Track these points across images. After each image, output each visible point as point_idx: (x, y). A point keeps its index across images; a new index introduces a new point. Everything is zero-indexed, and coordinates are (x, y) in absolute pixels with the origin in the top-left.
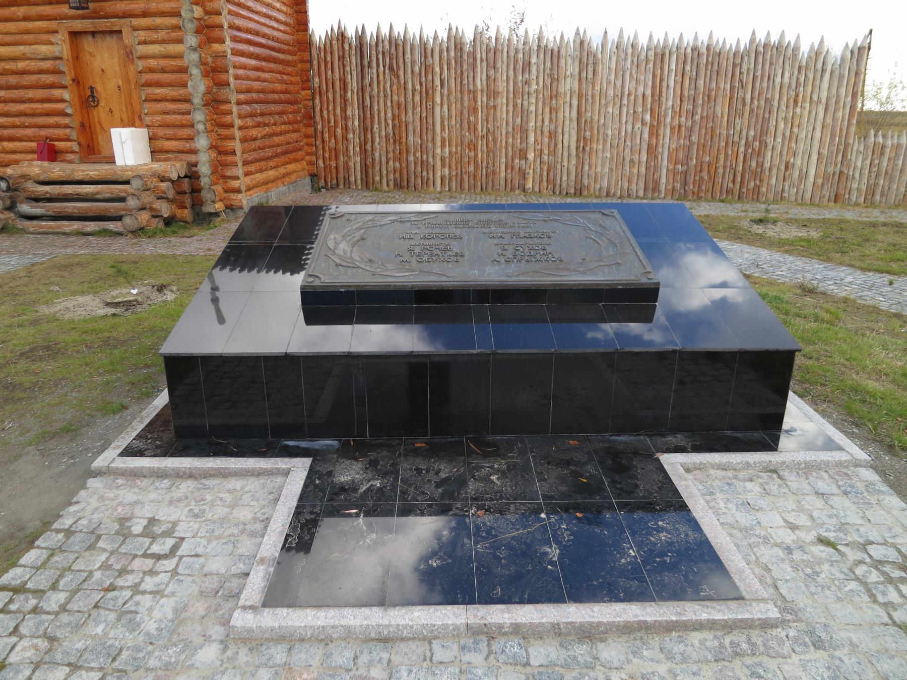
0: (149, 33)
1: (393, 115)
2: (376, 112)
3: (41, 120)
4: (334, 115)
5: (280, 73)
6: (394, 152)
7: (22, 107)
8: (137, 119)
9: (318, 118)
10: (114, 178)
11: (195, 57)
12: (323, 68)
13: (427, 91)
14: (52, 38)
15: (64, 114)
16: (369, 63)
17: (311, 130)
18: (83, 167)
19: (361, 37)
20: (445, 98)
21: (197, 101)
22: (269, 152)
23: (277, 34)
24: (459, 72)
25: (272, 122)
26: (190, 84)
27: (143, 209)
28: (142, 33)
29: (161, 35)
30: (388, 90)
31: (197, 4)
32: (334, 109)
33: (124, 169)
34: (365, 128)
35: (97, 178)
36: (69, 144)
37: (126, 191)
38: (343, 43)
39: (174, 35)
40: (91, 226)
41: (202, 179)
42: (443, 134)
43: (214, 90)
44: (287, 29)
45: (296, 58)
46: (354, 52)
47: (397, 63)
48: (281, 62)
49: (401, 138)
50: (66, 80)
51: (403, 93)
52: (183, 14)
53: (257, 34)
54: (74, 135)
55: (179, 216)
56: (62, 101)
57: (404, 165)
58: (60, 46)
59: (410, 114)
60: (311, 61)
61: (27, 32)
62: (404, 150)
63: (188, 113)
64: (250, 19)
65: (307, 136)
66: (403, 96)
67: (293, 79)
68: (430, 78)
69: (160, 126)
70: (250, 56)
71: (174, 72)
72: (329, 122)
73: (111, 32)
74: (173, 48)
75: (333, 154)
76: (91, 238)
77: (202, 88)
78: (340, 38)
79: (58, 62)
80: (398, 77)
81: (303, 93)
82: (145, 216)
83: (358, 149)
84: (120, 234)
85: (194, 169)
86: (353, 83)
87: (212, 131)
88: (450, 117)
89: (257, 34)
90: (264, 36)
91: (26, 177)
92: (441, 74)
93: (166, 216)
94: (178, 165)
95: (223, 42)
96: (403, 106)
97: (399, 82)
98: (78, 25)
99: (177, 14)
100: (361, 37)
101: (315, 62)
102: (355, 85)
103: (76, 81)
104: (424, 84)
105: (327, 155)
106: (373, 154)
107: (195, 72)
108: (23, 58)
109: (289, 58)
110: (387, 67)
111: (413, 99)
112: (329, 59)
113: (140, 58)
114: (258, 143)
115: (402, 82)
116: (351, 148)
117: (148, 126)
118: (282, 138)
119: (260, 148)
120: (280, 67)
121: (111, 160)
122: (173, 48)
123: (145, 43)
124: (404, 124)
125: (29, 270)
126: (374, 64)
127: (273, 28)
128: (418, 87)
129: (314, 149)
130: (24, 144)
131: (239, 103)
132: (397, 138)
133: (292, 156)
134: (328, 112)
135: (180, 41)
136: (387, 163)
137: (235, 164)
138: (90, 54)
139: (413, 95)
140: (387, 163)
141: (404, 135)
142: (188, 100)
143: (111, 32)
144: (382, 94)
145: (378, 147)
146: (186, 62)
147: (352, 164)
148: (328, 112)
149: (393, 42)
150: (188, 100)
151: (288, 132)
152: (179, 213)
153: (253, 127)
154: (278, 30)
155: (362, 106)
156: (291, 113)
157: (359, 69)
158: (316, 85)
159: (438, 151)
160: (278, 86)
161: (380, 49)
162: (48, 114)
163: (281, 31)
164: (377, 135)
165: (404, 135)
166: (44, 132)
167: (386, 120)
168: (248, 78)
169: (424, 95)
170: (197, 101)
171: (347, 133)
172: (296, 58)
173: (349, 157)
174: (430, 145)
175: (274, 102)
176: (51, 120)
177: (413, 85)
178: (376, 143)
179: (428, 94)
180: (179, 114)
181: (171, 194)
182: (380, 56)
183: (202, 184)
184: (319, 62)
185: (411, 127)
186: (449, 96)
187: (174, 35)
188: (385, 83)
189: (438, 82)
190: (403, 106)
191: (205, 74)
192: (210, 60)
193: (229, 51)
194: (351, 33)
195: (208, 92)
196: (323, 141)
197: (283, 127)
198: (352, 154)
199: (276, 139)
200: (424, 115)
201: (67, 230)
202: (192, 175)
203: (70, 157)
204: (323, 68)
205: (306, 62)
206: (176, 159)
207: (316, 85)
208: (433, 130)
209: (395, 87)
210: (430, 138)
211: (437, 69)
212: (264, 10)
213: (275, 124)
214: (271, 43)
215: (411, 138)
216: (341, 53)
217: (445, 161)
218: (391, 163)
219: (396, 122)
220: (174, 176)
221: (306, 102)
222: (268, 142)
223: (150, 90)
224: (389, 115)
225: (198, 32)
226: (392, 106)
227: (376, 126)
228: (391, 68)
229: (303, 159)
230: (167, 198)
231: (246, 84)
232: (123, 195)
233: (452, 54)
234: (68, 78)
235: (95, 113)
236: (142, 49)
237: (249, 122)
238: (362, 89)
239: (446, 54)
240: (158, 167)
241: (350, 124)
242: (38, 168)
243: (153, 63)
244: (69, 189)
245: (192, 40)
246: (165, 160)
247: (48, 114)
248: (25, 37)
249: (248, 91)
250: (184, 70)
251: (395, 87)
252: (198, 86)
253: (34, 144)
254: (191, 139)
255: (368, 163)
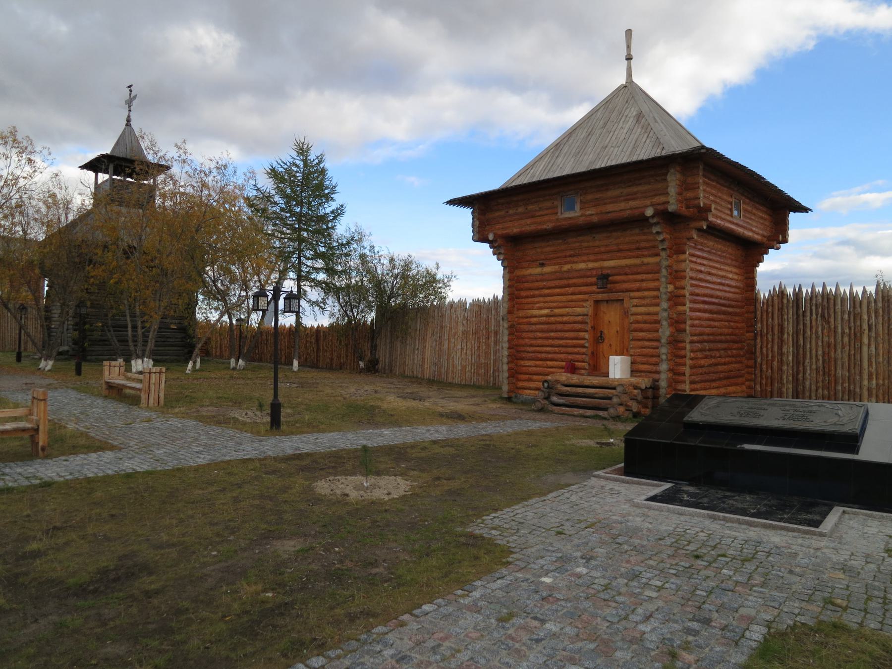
0: (640, 300)
1: (824, 353)
2: (808, 350)
3: (570, 350)
4: (772, 351)
5: (728, 321)
6: (823, 382)
7: (561, 342)
8: (625, 351)
9: (758, 353)
10: (607, 385)
11: (665, 314)
12: (765, 316)
13: (855, 334)
14: (584, 304)
15: (584, 347)
16: (804, 312)
17: (751, 362)
18: (590, 378)
19: (798, 294)
20: (872, 339)
21: (663, 341)
22: (713, 377)
23: (731, 295)
24: (886, 318)
25: (718, 355)
26: (660, 330)
27: (621, 405)
28: (635, 301)
29: (647, 301)
30: (820, 333)
31: (670, 283)
32: (772, 347)
33: (614, 380)
34: (799, 361)
35: (598, 385)
36: (583, 364)
37: (612, 394)
38: (782, 298)
39: (654, 301)
40: (589, 413)
41: (661, 390)
42: (870, 369)
43: (676, 334)
44: (737, 290)
45: (744, 310)
46: (791, 305)
47: (828, 312)
48: (730, 314)
49: (830, 370)
50: (588, 327)
51: (833, 335)
52: (661, 289)
53: (712, 296)
54: (587, 359)
55: (643, 413)
56: (584, 339)
57: (832, 393)
58: (587, 308)
59: (839, 351)
60: (755, 312)
61: (572, 301)
62: (833, 380)
63: (657, 348)
64: (707, 288)
65: (748, 366)
66: (833, 337)
67: (739, 325)
68: (858, 323)
69: (639, 355)
70: (705, 311)
71: (651, 323)
72: (767, 356)
73: (618, 300)
74: (652, 309)
75: (769, 381)
76: (588, 419)
77: (668, 333)
78: (780, 295)
79: (585, 317)
80: (828, 323)
81: (747, 335)
82: (621, 409)
83: (791, 378)
84: (605, 419)
85: (657, 383)
86: (789, 328)
87: (671, 360)
88: (877, 354)
89: (712, 296)
90: (717, 297)
91: (557, 381)
92: (869, 321)
93: (634, 410)
94: (646, 380)
95: (684, 305)
96: (833, 345)
97: (829, 327)
98: (600, 297)
99: (658, 289)
100: (798, 294)
101: (759, 313)
102: (791, 329)
103: (593, 328)
104: (853, 328)
105: (764, 382)
106: (804, 383)
107: (665, 323)
108: (567, 315)
109: (738, 310)
110: (819, 316)
111: (842, 340)
112: (770, 310)
113: (632, 315)
114: (704, 369)
115: (833, 327)
116: (785, 377)
117: (631, 355)
118: (725, 367)
119: (706, 373)
120: (729, 318)
121: (607, 375)
122: (652, 309)
123: (636, 306)
124: (833, 360)
125: (557, 428)
126: (808, 314)
127: (725, 291)
128: (847, 331)
129: (753, 376)
130: (558, 363)
131: (692, 342)
132: (827, 370)
133: (732, 381)
134: (767, 349)
135: (657, 305)
136: (817, 390)
137: (684, 382)
138: (604, 312)
139: (842, 337)
140: (817, 390)
141: (833, 368)
142: (658, 340)
143: (618, 300)
144: (814, 336)
145: (809, 377)
146: (659, 317)
147: (784, 390)
148: (767, 349)
149: (825, 297)
150: (658, 340)
151: (732, 363)
152: (643, 411)
153: (701, 358)
154: (729, 292)
155: (796, 345)
156: (735, 349)
157: (795, 317)
158: (758, 329)
159: (866, 382)
160: (726, 331)
161: (814, 302)
162: (574, 346)
163: (732, 293)
164: (808, 368)
165: (833, 368)
166: (570, 357)
167: (816, 356)
168: (701, 326)
169: (853, 337)
170: (663, 341)
171: (782, 366)
172: (744, 310)
173: (783, 384)
174: (858, 378)
175: (721, 342)
176: (576, 350)
177: (843, 329)
178: (807, 374)
179: (856, 337)
180: (652, 348)
181: (640, 397)
182: (814, 308)
183: (661, 393)
184: (762, 313)
185: (839, 363)
186: (876, 338)
187: (654, 301)
188: (817, 327)
189: (865, 327)
190: (833, 345)
191: (671, 325)
192: (675, 316)
193: (688, 310)
194: (790, 291)
195: (672, 335)
196: (761, 371)
197: (727, 359)
198: (785, 382)
199: (720, 368)
200: (852, 352)
201: (576, 413)
202: (655, 387)
203: (583, 371)
204: (765, 316)
205: (752, 312)
206: (646, 376)
207: (758, 329)
208: (861, 365)
209: (826, 331)
210: (858, 372)
211: (865, 317)
212: (719, 281)
213: (719, 357)
214: (722, 301)
215: (839, 372)
216: (780, 306)
217: (872, 392)
218: (820, 391)
219: (826, 358)
220: (643, 387)
221: (749, 342)
222: (712, 369)
223: (635, 334)
224: (820, 352)
225: (669, 300)
226: (823, 345)
227: (808, 361)
228: (823, 316)
229: (743, 384)
230: (637, 400)
231: (698, 330)
232: (610, 395)
233: (880, 304)
234: (589, 326)
235: (601, 346)
236: (634, 310)
237: (699, 355)
238: (797, 332)
239: (873, 305)
240: (633, 380)
241: (784, 359)
242: (564, 377)
243: (639, 318)
244: (580, 390)
245: (665, 305)
246: (639, 377)
247: (574, 346)
248: (570, 303)
249: (701, 334)
250: (658, 322)
251: (826, 331)
252: (665, 332)
253: (564, 363)
254: (657, 364)
255: (799, 390)
